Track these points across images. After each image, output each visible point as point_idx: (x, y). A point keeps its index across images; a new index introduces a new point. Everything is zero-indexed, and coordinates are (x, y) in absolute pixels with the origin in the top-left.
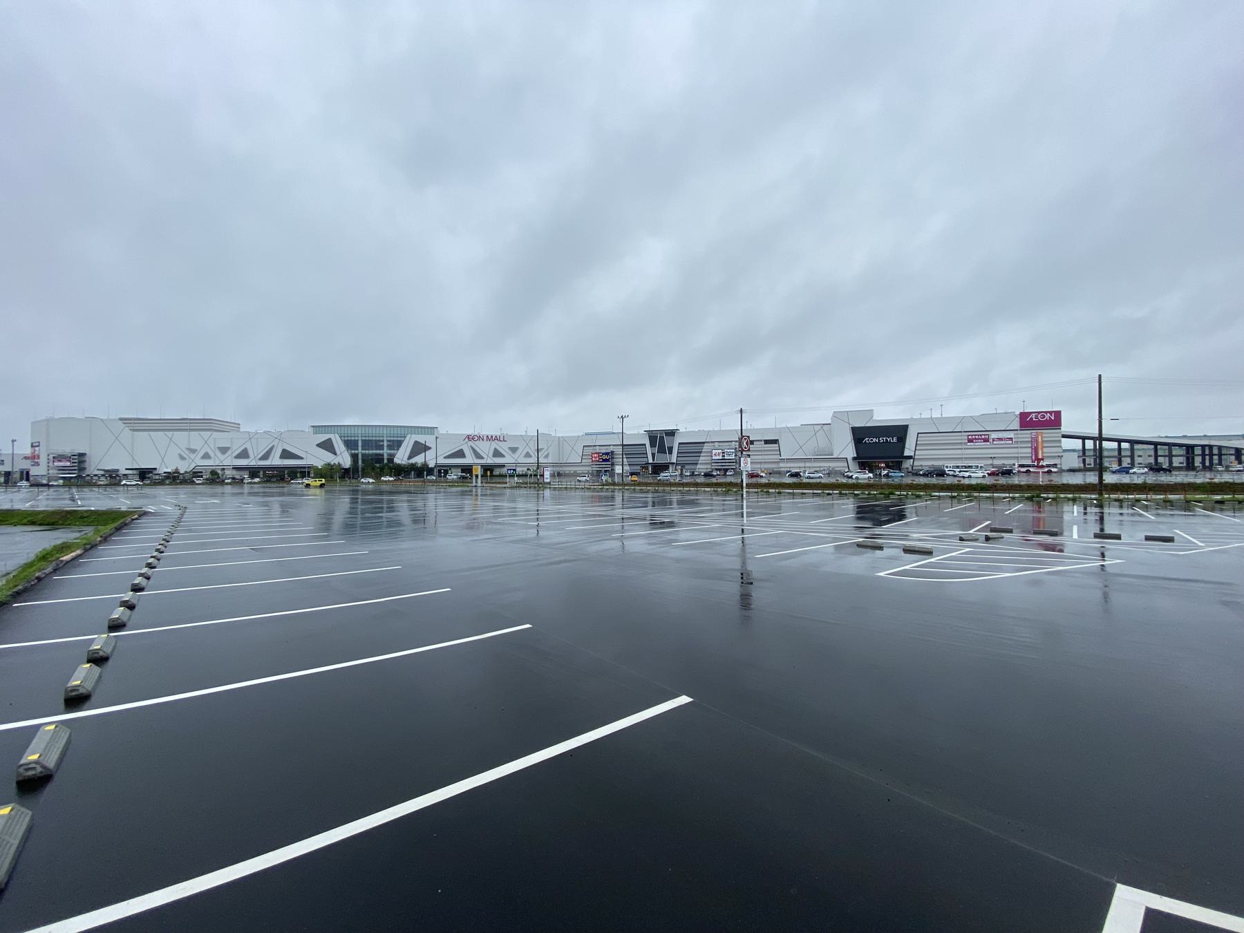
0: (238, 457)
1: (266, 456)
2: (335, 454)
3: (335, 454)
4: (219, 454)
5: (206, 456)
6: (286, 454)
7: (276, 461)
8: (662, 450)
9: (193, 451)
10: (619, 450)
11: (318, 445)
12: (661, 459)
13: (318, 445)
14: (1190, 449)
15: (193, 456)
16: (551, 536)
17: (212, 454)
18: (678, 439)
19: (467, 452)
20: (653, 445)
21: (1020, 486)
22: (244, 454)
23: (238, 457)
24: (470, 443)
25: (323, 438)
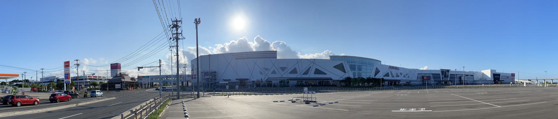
0: (291, 73)
1: (306, 73)
2: (345, 72)
3: (345, 72)
4: (280, 70)
5: (274, 72)
6: (317, 72)
7: (312, 75)
8: (445, 76)
9: (267, 69)
10: (431, 76)
11: (335, 67)
12: (445, 79)
13: (335, 67)
14: (215, 76)
15: (266, 72)
16: (250, 43)
17: (277, 71)
18: (450, 73)
19: (390, 74)
20: (442, 74)
21: (362, 80)
22: (294, 71)
23: (291, 73)
24: (391, 70)
25: (338, 63)
